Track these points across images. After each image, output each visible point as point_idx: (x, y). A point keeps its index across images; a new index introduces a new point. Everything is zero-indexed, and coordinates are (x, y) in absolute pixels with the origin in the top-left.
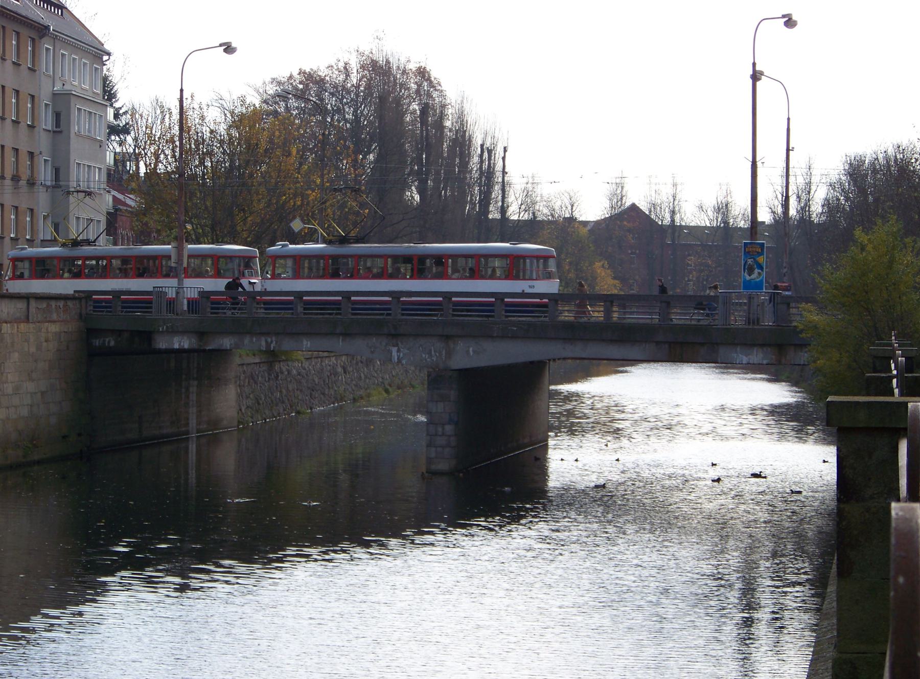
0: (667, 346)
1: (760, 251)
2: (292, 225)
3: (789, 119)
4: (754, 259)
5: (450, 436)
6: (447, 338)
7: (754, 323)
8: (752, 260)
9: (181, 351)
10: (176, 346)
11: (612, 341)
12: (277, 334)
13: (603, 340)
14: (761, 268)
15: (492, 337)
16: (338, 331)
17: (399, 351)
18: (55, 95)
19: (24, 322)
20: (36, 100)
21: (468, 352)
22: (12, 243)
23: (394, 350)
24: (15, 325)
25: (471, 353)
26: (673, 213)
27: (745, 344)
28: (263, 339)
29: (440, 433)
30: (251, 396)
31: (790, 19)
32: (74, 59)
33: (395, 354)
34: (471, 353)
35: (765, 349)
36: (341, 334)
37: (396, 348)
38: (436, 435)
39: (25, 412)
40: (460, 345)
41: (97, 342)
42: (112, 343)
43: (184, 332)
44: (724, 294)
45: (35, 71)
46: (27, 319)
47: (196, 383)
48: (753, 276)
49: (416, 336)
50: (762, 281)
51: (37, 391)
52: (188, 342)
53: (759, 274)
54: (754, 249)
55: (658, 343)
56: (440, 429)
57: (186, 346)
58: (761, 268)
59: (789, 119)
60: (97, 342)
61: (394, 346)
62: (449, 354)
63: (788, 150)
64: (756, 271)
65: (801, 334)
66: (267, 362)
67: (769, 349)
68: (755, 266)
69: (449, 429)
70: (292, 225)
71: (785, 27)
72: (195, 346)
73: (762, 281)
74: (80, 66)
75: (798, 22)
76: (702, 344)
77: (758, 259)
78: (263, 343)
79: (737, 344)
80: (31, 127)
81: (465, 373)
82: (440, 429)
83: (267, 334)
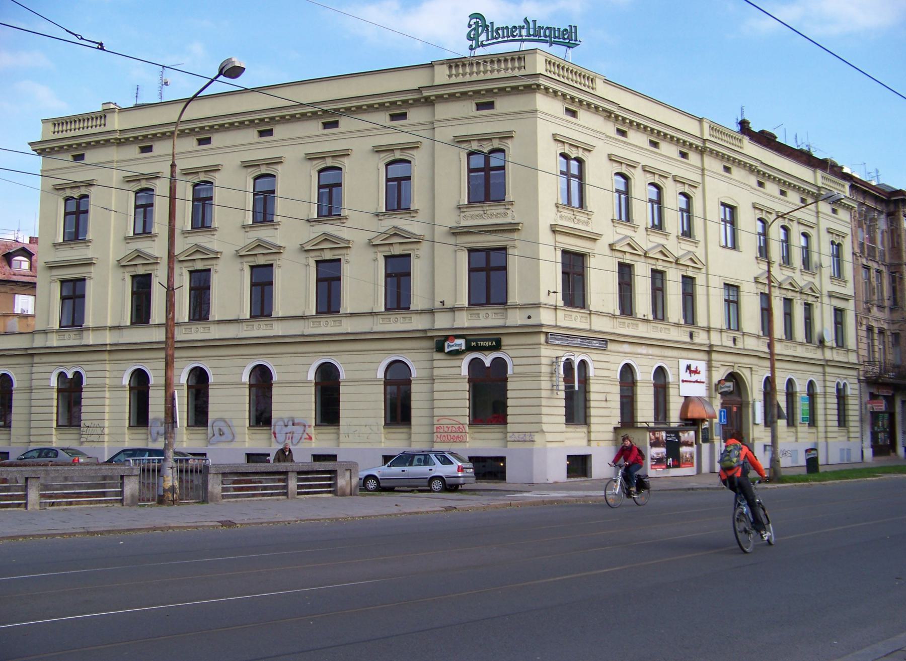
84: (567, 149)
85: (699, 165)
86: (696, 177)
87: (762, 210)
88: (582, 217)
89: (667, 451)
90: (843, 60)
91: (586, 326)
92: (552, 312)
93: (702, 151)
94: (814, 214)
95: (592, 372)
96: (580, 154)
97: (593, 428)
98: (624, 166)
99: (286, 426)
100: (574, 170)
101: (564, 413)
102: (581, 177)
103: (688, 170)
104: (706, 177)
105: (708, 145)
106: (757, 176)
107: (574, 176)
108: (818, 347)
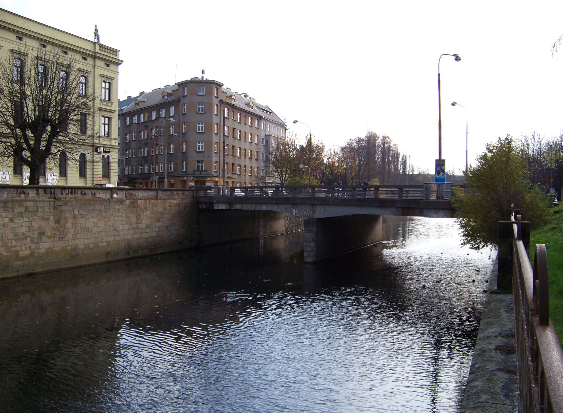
0: (401, 209)
2: (300, 166)
3: (439, 75)
5: (313, 247)
6: (313, 205)
7: (439, 198)
9: (222, 210)
10: (220, 208)
11: (378, 207)
12: (254, 204)
13: (374, 206)
15: (330, 205)
16: (274, 202)
17: (295, 211)
18: (266, 136)
19: (153, 199)
20: (259, 136)
21: (321, 211)
22: (249, 178)
23: (294, 210)
24: (148, 201)
25: (322, 211)
26: (453, 172)
27: (435, 209)
28: (250, 205)
29: (309, 246)
30: (296, 222)
31: (458, 56)
32: (274, 127)
33: (294, 211)
34: (322, 211)
35: (445, 211)
36: (275, 204)
37: (294, 209)
38: (307, 247)
39: (154, 234)
40: (318, 208)
41: (200, 207)
42: (205, 207)
43: (223, 203)
44: (426, 185)
45: (241, 123)
46: (157, 198)
47: (263, 219)
48: (440, 176)
49: (301, 204)
50: (444, 178)
51: (163, 226)
52: (225, 207)
55: (397, 208)
56: (309, 244)
57: (224, 208)
59: (439, 75)
60: (200, 207)
61: (294, 208)
62: (314, 212)
63: (467, 133)
64: (442, 173)
65: (453, 205)
66: (33, 226)
67: (447, 211)
69: (313, 244)
70: (300, 166)
71: (455, 61)
72: (228, 208)
73: (444, 178)
74: (272, 128)
75: (461, 61)
76: (417, 208)
77: (442, 167)
78: (250, 207)
79: (431, 209)
80: (251, 143)
81: (319, 220)
82: (309, 244)
83: (251, 203)
84: (105, 79)
85: (93, 64)
86: (90, 69)
87: (104, 77)
88: (110, 104)
89: (432, 202)
90: (467, 137)
91: (109, 143)
92: (98, 139)
93: (94, 57)
94: (93, 67)
95: (111, 160)
96: (110, 81)
97: (68, 178)
98: (110, 79)
99: (51, 176)
100: (107, 86)
101: (30, 171)
102: (109, 89)
103: (87, 65)
104: (96, 69)
105: (97, 55)
106: (105, 62)
107: (107, 89)
108: (264, 161)
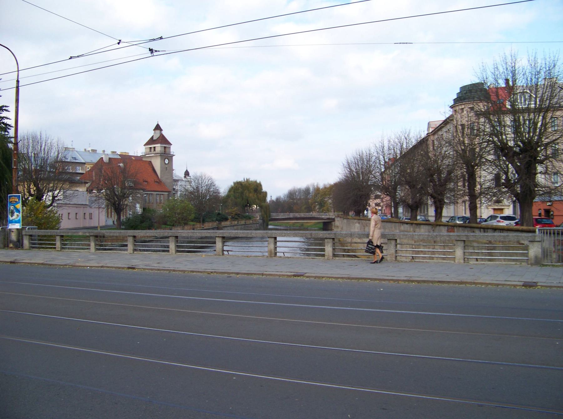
1: (17, 200)
4: (14, 206)
8: (13, 206)
14: (18, 211)
53: (18, 215)
54: (14, 200)
58: (18, 211)
64: (16, 214)
68: (15, 211)
